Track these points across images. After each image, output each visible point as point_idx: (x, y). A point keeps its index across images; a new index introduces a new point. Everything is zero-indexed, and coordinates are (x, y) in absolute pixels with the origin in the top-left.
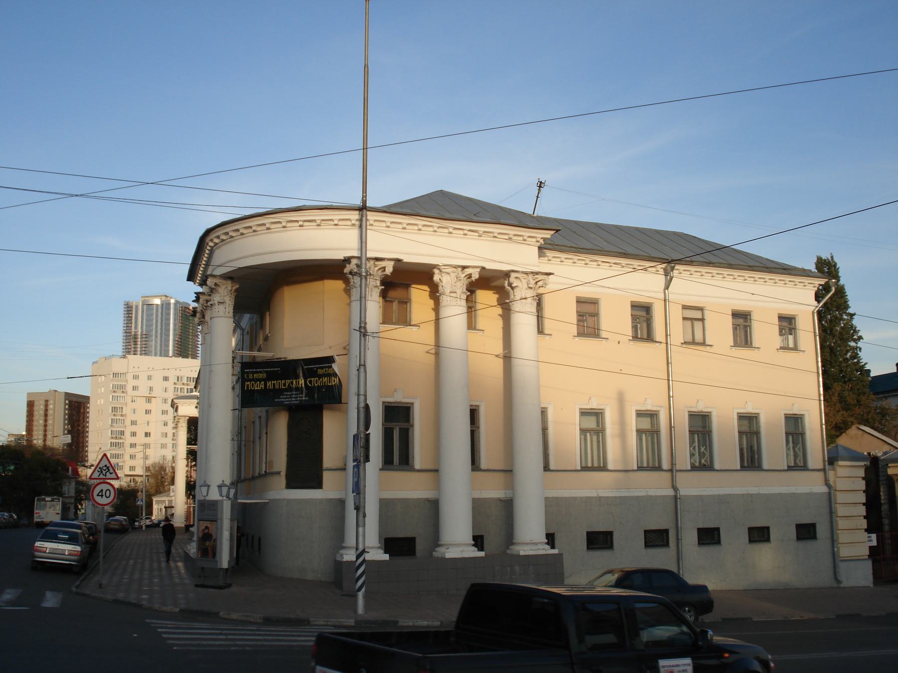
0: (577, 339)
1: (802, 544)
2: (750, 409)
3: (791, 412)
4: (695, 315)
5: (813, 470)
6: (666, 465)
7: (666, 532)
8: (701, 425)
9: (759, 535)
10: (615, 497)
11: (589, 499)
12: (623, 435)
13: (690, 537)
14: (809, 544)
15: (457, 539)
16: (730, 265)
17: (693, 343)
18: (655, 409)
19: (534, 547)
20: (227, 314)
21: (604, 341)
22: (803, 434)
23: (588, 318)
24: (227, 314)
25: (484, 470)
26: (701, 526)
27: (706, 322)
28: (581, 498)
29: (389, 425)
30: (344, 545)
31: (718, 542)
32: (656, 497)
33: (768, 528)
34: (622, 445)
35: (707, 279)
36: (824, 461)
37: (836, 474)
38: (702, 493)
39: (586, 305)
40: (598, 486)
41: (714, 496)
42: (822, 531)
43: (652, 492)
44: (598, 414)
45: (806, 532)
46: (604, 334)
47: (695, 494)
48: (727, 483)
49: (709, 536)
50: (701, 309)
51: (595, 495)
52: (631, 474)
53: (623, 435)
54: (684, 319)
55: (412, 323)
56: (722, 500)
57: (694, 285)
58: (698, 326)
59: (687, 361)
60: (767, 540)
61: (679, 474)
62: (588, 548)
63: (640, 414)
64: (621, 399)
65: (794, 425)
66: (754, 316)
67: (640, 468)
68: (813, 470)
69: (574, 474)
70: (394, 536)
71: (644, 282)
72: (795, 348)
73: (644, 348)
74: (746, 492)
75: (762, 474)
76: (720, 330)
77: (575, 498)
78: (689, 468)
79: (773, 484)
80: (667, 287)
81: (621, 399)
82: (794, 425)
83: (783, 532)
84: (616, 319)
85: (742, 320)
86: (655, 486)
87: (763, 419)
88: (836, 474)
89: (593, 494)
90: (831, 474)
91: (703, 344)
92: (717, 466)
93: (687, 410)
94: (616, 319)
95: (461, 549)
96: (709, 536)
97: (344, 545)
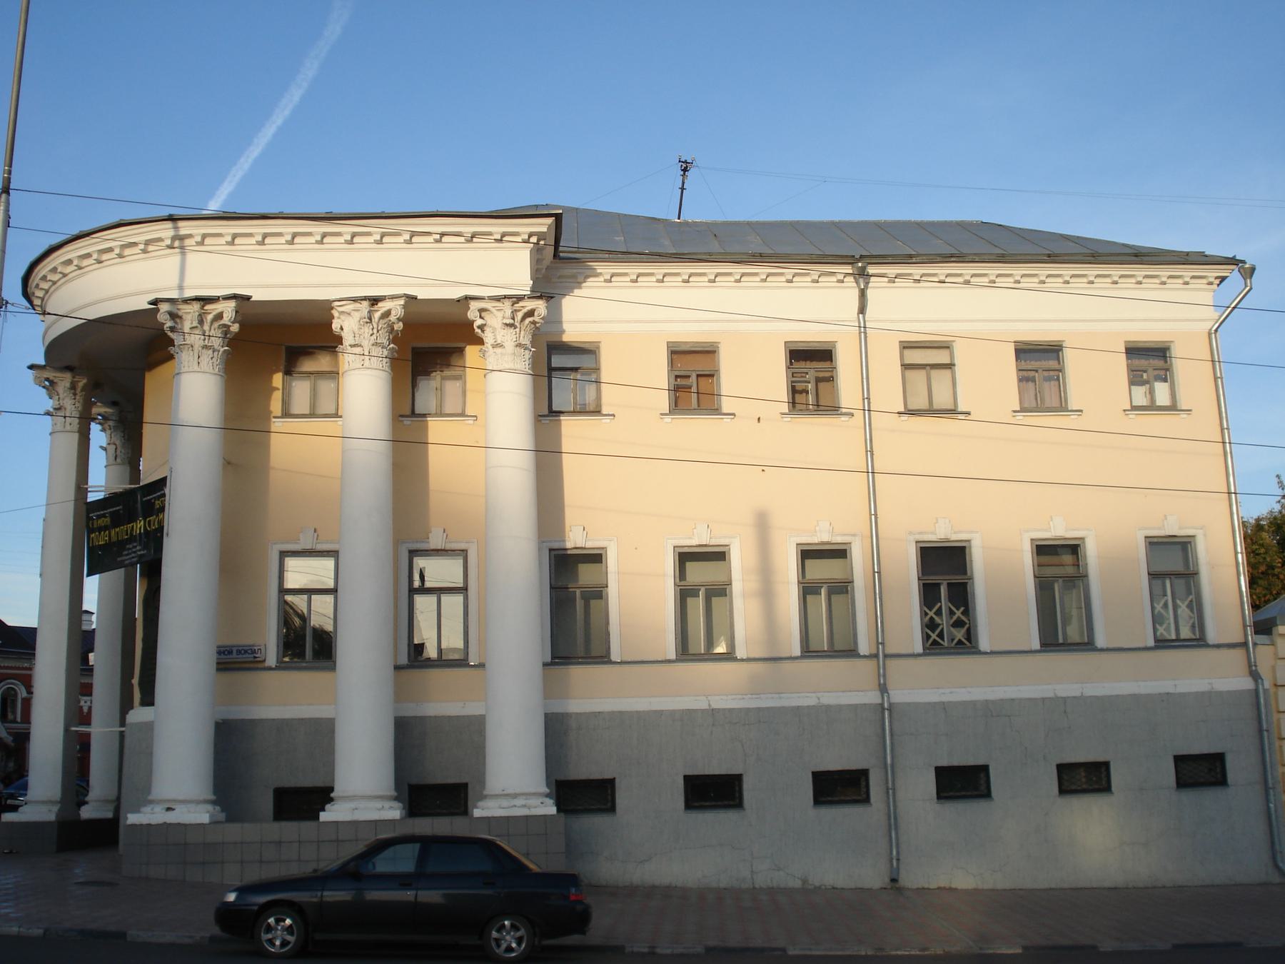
0: (668, 419)
1: (1189, 797)
2: (1058, 529)
3: (1162, 533)
4: (927, 359)
5: (1218, 646)
6: (864, 647)
7: (864, 773)
8: (944, 567)
9: (1083, 778)
10: (748, 710)
11: (690, 713)
12: (767, 592)
13: (918, 786)
14: (1208, 798)
15: (363, 790)
16: (911, 256)
17: (931, 411)
18: (839, 539)
19: (505, 803)
20: (68, 428)
21: (727, 419)
22: (1195, 574)
23: (693, 378)
24: (68, 428)
25: (1102, 650)
26: (944, 763)
27: (958, 369)
28: (673, 713)
29: (932, 579)
30: (150, 798)
31: (987, 794)
32: (840, 708)
33: (1106, 765)
34: (761, 608)
35: (1127, 288)
36: (1245, 626)
37: (1276, 654)
38: (944, 699)
39: (929, 351)
40: (713, 687)
41: (974, 703)
42: (1239, 768)
43: (829, 699)
44: (1182, 546)
45: (1201, 771)
46: (726, 405)
47: (1194, 689)
48: (1006, 675)
49: (963, 783)
50: (946, 346)
51: (705, 706)
52: (787, 666)
53: (767, 592)
54: (906, 367)
55: (725, 410)
56: (990, 711)
57: (913, 302)
58: (941, 378)
59: (907, 443)
60: (1106, 788)
61: (892, 664)
62: (939, 797)
63: (808, 554)
64: (762, 526)
65: (1172, 562)
66: (1176, 351)
67: (808, 651)
68: (1218, 646)
69: (911, 661)
70: (299, 785)
71: (814, 303)
72: (1173, 408)
73: (813, 428)
74: (1051, 695)
75: (467, 669)
76: (988, 381)
77: (660, 713)
78: (1151, 643)
79: (1118, 676)
80: (862, 310)
81: (762, 526)
82: (1172, 562)
83: (1142, 769)
84: (754, 377)
85: (1039, 361)
86: (839, 686)
87: (1092, 551)
88: (1276, 654)
89: (701, 704)
90: (1264, 655)
91: (952, 412)
92: (1100, 641)
93: (913, 538)
94: (754, 377)
95: (352, 805)
96: (963, 783)
97: (150, 798)
